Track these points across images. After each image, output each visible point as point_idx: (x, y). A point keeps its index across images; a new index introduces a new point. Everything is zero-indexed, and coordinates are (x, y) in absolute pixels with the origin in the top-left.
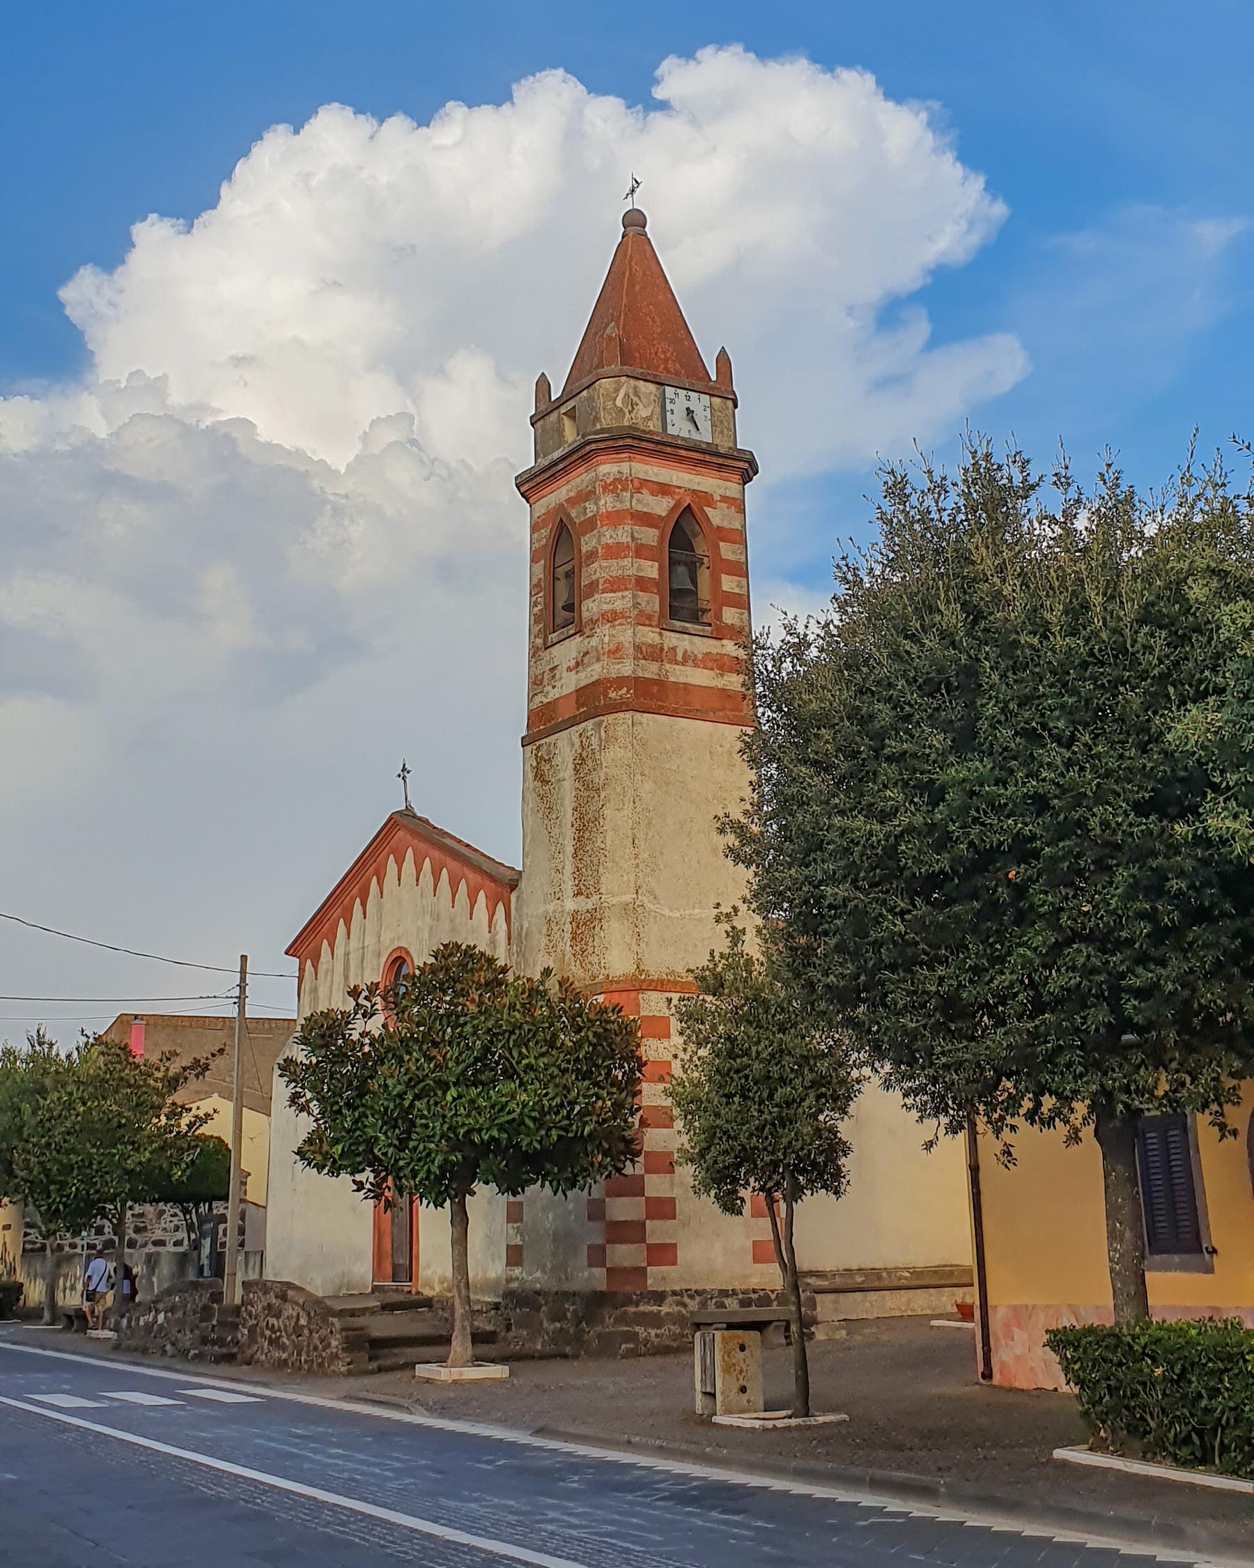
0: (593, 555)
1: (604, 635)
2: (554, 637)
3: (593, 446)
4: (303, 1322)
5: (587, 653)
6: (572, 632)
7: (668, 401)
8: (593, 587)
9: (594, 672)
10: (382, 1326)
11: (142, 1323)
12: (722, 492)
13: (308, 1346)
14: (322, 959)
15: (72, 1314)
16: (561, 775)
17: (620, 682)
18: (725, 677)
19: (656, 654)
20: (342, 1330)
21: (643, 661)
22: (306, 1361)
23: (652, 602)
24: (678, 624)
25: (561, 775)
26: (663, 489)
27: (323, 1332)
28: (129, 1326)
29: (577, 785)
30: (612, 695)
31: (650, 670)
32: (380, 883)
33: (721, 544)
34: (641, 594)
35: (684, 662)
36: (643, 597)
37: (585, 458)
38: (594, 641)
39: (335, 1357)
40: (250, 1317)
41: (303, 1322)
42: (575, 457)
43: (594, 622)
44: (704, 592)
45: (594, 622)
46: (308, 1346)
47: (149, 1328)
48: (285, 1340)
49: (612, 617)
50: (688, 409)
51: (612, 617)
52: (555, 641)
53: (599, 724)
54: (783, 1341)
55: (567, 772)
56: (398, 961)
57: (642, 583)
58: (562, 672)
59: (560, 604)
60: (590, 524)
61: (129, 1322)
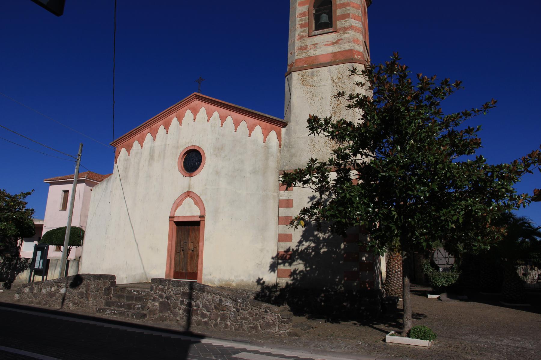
5: (341, 39)
11: (44, 291)
25: (323, 84)
38: (346, 36)
52: (317, 34)
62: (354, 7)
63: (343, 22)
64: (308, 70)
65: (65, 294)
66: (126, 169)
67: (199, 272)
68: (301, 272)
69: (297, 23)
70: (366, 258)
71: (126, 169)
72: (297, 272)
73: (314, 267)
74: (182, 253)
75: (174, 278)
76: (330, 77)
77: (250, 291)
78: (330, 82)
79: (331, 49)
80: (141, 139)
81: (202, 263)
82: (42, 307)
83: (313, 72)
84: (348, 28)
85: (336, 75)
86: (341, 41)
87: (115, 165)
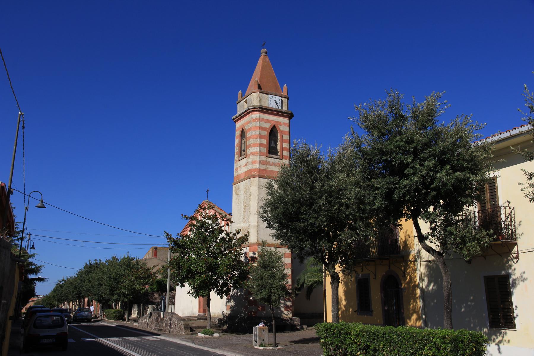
1: (250, 159)
2: (240, 158)
8: (249, 146)
9: (249, 167)
10: (195, 324)
17: (255, 169)
19: (266, 163)
23: (265, 150)
24: (271, 155)
26: (268, 121)
31: (263, 167)
35: (272, 165)
37: (249, 113)
38: (249, 160)
39: (182, 331)
43: (249, 155)
44: (279, 148)
45: (249, 155)
47: (145, 323)
49: (253, 154)
51: (253, 154)
54: (31, 236)
55: (242, 192)
56: (114, 258)
57: (261, 145)
58: (242, 167)
60: (249, 130)
62: (253, 138)
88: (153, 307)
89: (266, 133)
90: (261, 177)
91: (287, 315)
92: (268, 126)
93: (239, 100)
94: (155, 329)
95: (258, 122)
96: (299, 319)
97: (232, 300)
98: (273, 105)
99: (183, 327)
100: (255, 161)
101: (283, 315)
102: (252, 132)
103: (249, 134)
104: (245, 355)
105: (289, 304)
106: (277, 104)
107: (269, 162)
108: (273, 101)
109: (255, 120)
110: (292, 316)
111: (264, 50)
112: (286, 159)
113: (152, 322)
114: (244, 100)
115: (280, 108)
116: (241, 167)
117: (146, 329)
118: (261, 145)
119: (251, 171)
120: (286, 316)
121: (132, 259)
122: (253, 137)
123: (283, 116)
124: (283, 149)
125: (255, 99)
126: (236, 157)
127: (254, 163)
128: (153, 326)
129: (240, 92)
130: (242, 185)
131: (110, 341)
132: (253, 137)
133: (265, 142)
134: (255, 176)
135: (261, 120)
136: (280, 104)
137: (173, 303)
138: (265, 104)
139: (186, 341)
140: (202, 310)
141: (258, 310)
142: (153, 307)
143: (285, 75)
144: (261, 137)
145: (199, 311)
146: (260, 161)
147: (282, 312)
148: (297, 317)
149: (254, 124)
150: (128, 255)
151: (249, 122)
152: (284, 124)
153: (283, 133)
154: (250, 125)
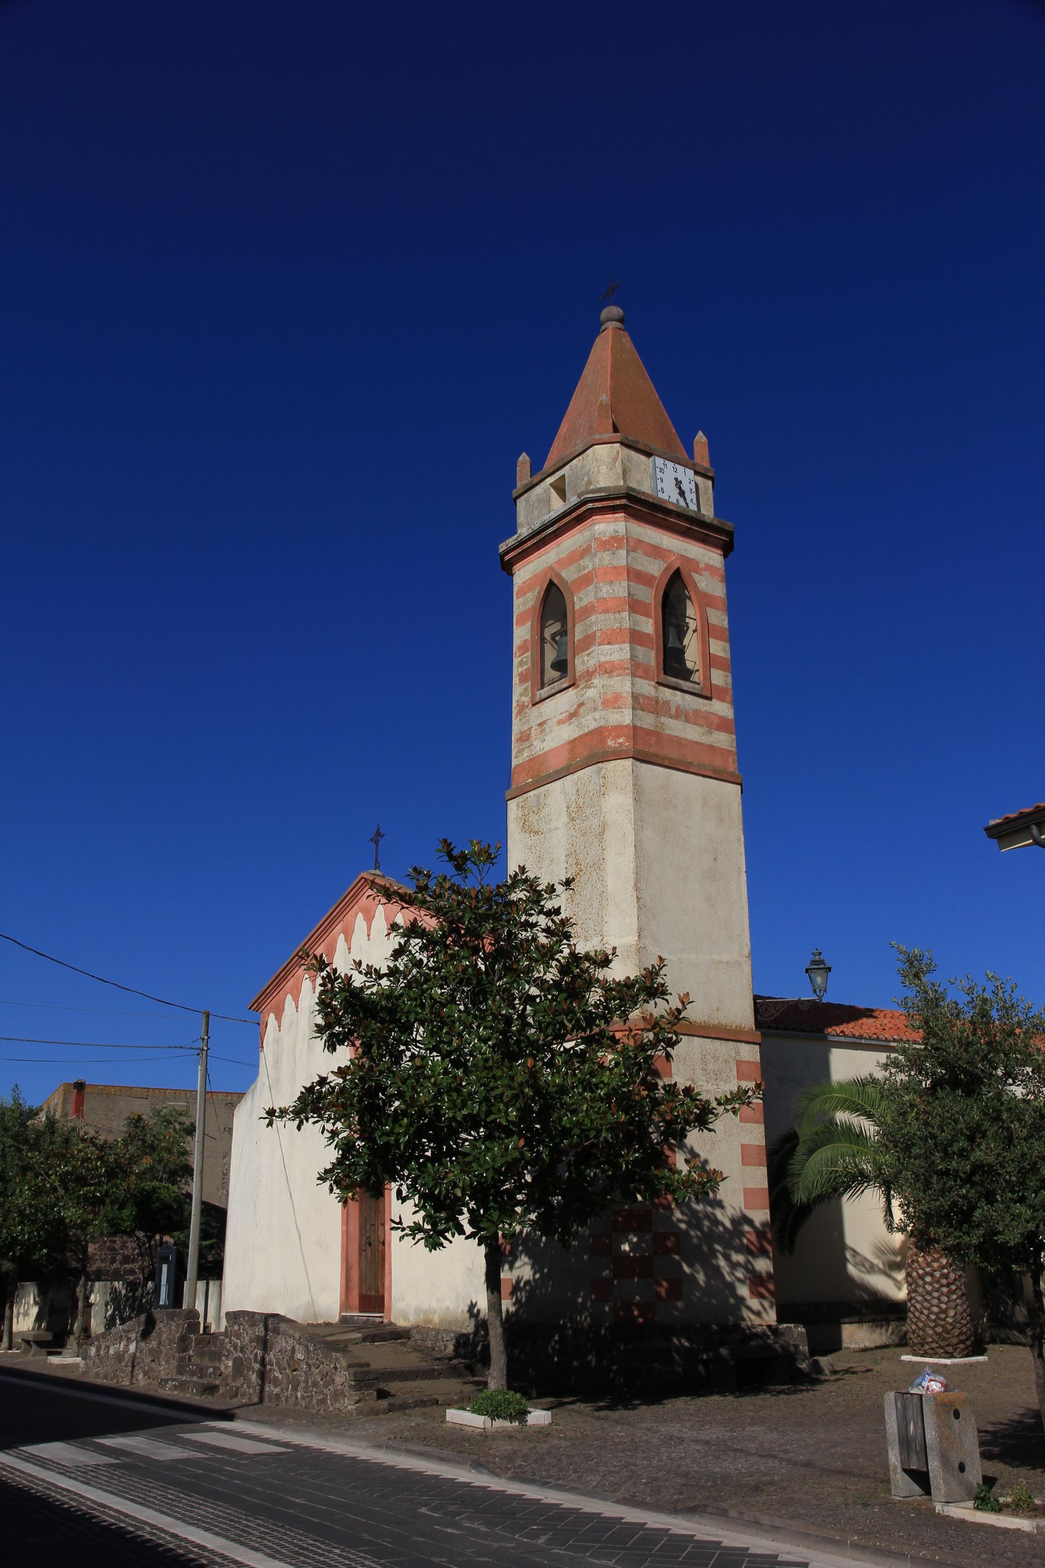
0: (588, 611)
3: (590, 505)
4: (299, 1356)
5: (582, 704)
6: (565, 685)
7: (658, 470)
8: (589, 641)
9: (590, 722)
11: (112, 1352)
12: (706, 560)
13: (306, 1382)
14: (286, 1013)
15: (30, 1338)
16: (553, 825)
17: (619, 729)
18: (714, 735)
19: (657, 708)
20: (349, 1366)
21: (640, 712)
22: (303, 1397)
23: (650, 657)
24: (672, 680)
25: (553, 825)
26: (656, 552)
27: (325, 1368)
28: (98, 1354)
29: (572, 832)
30: (610, 743)
31: (647, 721)
32: (348, 940)
33: (708, 609)
34: (638, 647)
35: (677, 717)
36: (641, 651)
37: (580, 520)
38: (591, 693)
39: (338, 1395)
40: (235, 1348)
41: (299, 1356)
42: (568, 518)
43: (589, 674)
45: (589, 674)
46: (306, 1382)
47: (119, 1357)
48: (277, 1374)
49: (608, 669)
50: (676, 479)
51: (608, 669)
52: (543, 696)
53: (600, 770)
59: (548, 664)
60: (586, 580)
61: (98, 1349)
62: (606, 611)
63: (586, 658)
64: (532, 793)
65: (135, 1354)
66: (277, 1061)
67: (386, 1294)
68: (527, 1283)
69: (515, 672)
70: (634, 1247)
71: (277, 1061)
72: (522, 1284)
73: (546, 1270)
74: (369, 1249)
75: (361, 1311)
76: (564, 805)
77: (446, 1331)
78: (564, 818)
79: (567, 733)
80: (295, 991)
81: (390, 1274)
82: (105, 1382)
83: (538, 796)
84: (593, 672)
85: (573, 798)
86: (583, 708)
87: (262, 1054)
88: (114, 1291)
89: (650, 596)
90: (642, 758)
91: (758, 1314)
92: (656, 568)
93: (520, 484)
94: (182, 1386)
95: (623, 553)
96: (801, 1329)
97: (524, 1259)
98: (669, 494)
99: (342, 1378)
100: (617, 697)
101: (746, 1313)
102: (597, 590)
103: (580, 600)
104: (914, 1559)
105: (763, 1265)
106: (682, 493)
107: (667, 703)
108: (670, 481)
109: (611, 543)
110: (780, 1320)
111: (615, 311)
112: (722, 699)
113: (155, 1355)
114: (550, 480)
115: (693, 507)
116: (544, 724)
117: (125, 1383)
118: (636, 637)
119: (599, 733)
120: (756, 1320)
121: (33, 1113)
122: (606, 607)
123: (704, 540)
124: (710, 661)
125: (604, 469)
126: (519, 692)
127: (611, 702)
128: (165, 1368)
129: (524, 457)
130: (557, 795)
131: (43, 1463)
132: (606, 607)
133: (649, 626)
134: (618, 755)
135: (634, 545)
136: (690, 496)
137: (212, 1269)
138: (644, 486)
139: (410, 1452)
140: (355, 1299)
141: (658, 1294)
142: (114, 1291)
143: (686, 400)
144: (635, 606)
145: (345, 1305)
146: (635, 697)
147: (741, 1300)
148: (797, 1321)
149: (605, 558)
150: (16, 1099)
151: (585, 552)
152: (709, 567)
153: (706, 600)
154: (588, 564)
